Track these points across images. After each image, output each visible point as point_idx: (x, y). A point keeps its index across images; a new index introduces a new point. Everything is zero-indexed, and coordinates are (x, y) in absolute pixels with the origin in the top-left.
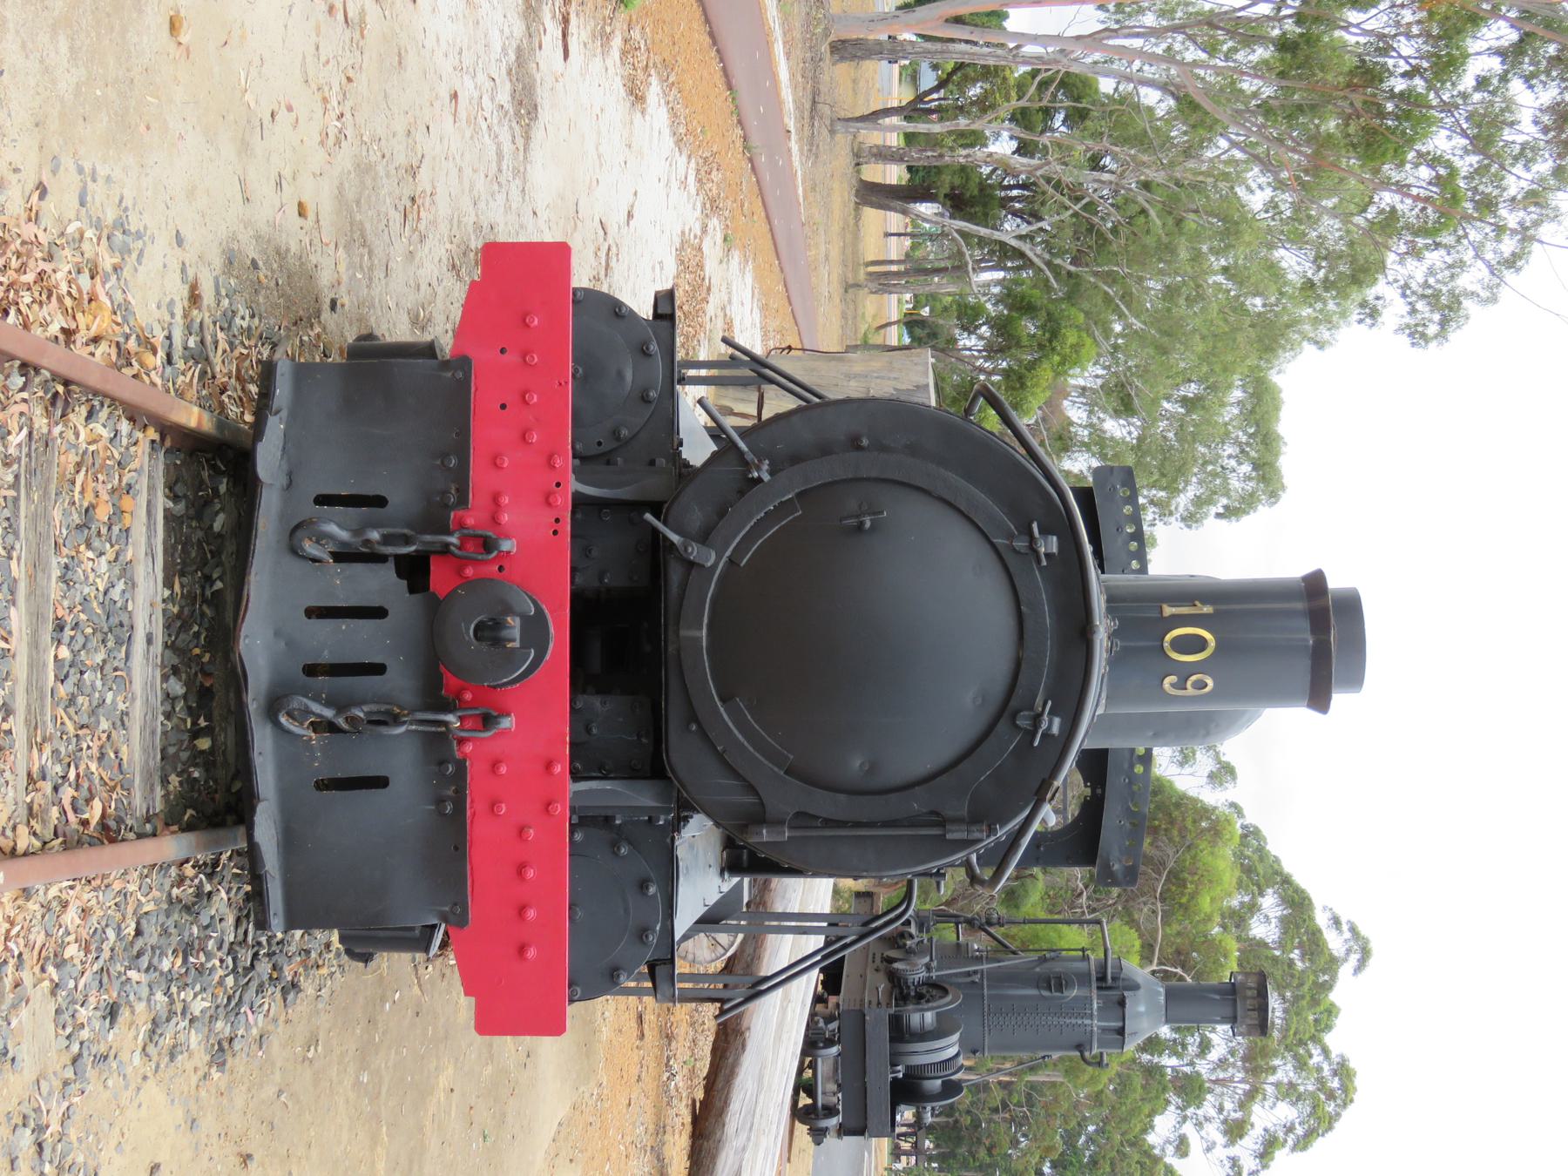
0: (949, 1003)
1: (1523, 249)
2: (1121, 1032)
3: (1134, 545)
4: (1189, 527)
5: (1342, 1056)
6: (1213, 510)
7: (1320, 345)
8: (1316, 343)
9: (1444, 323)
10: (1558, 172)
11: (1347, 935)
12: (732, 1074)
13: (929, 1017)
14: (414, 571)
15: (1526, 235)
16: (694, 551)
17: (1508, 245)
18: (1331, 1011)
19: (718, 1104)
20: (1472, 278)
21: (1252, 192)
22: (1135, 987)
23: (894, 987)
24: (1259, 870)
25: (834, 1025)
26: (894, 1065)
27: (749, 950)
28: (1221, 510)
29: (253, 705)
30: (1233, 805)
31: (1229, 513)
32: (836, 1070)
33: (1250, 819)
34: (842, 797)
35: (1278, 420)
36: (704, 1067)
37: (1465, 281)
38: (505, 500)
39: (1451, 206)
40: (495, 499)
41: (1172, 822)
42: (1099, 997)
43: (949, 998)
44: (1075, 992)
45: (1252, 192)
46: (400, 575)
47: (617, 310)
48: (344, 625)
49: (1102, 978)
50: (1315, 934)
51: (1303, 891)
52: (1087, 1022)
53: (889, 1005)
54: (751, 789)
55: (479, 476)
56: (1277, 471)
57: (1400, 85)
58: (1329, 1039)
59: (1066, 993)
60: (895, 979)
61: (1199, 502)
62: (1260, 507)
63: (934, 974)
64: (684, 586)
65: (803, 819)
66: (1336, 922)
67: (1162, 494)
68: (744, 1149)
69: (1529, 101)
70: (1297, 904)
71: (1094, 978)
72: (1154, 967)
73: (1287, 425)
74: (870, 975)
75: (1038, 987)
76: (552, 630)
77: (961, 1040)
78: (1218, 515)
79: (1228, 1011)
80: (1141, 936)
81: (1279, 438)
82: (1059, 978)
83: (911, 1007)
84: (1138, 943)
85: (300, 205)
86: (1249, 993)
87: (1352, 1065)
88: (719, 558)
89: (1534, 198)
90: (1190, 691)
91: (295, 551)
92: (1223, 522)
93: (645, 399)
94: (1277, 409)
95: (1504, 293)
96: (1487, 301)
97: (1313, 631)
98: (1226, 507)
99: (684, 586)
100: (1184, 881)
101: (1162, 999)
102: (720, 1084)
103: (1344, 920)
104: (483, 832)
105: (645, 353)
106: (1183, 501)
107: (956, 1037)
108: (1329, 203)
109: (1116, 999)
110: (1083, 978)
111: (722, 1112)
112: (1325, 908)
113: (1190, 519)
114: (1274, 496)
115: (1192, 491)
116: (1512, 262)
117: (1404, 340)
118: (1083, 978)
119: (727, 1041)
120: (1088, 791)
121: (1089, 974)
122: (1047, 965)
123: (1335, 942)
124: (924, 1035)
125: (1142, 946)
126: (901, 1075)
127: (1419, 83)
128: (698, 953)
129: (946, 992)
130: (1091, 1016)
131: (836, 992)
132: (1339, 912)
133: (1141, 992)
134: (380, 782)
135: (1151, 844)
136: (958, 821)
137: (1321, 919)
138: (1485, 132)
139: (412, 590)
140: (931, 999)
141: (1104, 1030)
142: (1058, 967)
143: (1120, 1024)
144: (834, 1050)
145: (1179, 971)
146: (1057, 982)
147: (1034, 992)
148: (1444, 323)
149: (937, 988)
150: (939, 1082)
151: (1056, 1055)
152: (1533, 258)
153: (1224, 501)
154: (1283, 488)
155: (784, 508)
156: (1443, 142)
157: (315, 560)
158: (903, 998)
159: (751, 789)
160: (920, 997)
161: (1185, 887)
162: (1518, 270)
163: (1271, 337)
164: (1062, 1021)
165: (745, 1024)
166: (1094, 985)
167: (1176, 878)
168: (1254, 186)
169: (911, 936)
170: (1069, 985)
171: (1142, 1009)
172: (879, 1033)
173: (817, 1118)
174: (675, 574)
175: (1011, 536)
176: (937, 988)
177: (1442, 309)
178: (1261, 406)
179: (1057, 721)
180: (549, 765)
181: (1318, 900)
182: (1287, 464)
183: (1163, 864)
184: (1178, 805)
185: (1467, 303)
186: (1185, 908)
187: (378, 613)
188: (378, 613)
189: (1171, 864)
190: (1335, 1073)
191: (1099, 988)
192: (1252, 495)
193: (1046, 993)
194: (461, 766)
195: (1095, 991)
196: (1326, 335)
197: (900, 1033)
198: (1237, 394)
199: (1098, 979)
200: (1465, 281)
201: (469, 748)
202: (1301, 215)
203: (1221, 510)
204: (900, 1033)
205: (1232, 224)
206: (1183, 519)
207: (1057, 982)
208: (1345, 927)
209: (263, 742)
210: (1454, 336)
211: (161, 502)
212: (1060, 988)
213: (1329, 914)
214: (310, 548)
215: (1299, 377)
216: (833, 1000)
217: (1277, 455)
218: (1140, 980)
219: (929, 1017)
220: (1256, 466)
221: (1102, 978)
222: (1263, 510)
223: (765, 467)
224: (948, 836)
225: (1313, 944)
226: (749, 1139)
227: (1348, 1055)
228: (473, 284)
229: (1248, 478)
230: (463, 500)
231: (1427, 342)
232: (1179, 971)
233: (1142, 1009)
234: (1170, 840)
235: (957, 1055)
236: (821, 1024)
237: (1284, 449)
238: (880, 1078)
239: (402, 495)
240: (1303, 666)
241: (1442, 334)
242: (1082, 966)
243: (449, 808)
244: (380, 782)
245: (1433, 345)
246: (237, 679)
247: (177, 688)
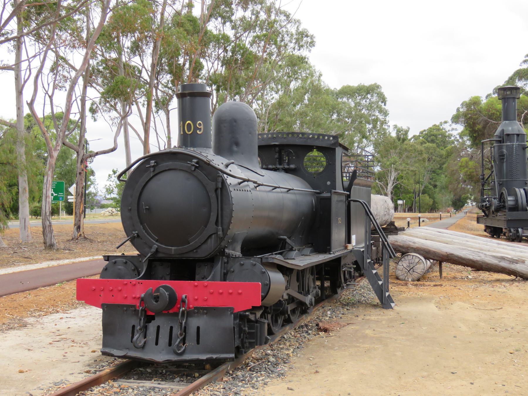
0: (505, 191)
1: (283, 13)
2: (518, 135)
3: (290, 136)
4: (388, 114)
6: (383, 106)
7: (321, 75)
8: (319, 77)
9: (307, 36)
10: (261, 3)
12: (461, 258)
14: (149, 319)
15: (279, 12)
16: (153, 250)
17: (283, 18)
19: (471, 262)
20: (292, 29)
21: (273, 98)
23: (500, 210)
25: (512, 230)
27: (422, 252)
28: (383, 104)
29: (174, 358)
30: (487, 97)
31: (384, 101)
33: (491, 92)
34: (212, 214)
35: (353, 86)
36: (460, 267)
37: (293, 30)
38: (134, 296)
39: (271, 35)
40: (135, 298)
43: (504, 192)
44: (505, 150)
45: (273, 98)
46: (150, 322)
47: (105, 269)
48: (160, 336)
49: (500, 142)
51: (515, 73)
52: (515, 146)
53: (505, 212)
54: (210, 236)
55: (129, 302)
56: (370, 86)
57: (230, 54)
59: (505, 153)
61: (381, 111)
62: (382, 91)
63: (497, 197)
64: (164, 253)
65: (217, 223)
67: (378, 123)
68: (485, 254)
69: (239, 13)
73: (354, 83)
74: (498, 218)
75: (503, 162)
76: (170, 286)
77: (519, 188)
78: (385, 105)
79: (511, 100)
81: (359, 86)
82: (500, 156)
83: (506, 205)
85: (92, 352)
86: (505, 93)
88: (155, 244)
89: (269, 11)
90: (202, 127)
91: (143, 347)
92: (387, 103)
93: (126, 263)
94: (349, 87)
95: (296, 17)
96: (300, 23)
97: (186, 97)
98: (382, 102)
99: (164, 253)
100: (491, 114)
101: (507, 122)
102: (465, 262)
103: (525, 59)
104: (212, 303)
105: (115, 262)
106: (381, 117)
107: (517, 190)
108: (275, 74)
110: (500, 148)
111: (473, 261)
112: (520, 65)
113: (386, 114)
114: (378, 87)
115: (377, 113)
116: (287, 16)
117: (313, 49)
118: (500, 148)
119: (451, 259)
120: (315, 150)
124: (516, 200)
127: (229, 48)
128: (422, 268)
129: (502, 193)
133: (505, 129)
134: (198, 328)
136: (216, 185)
138: (248, 26)
139: (154, 319)
141: (517, 141)
142: (497, 156)
144: (520, 230)
145: (523, 115)
147: (505, 164)
148: (307, 36)
152: (286, 10)
153: (380, 103)
154: (375, 84)
155: (144, 228)
156: (247, 39)
157: (145, 343)
158: (504, 207)
159: (210, 236)
160: (504, 202)
161: (494, 113)
162: (290, 14)
163: (317, 90)
165: (445, 254)
167: (491, 116)
168: (272, 97)
169: (486, 205)
170: (502, 152)
171: (510, 128)
172: (516, 215)
174: (160, 255)
175: (150, 172)
177: (303, 38)
178: (348, 92)
179: (193, 160)
180: (196, 286)
181: (518, 68)
182: (367, 82)
183: (486, 120)
185: (301, 29)
187: (158, 327)
188: (158, 327)
189: (486, 118)
191: (503, 142)
192: (378, 94)
193: (505, 160)
194: (195, 308)
195: (504, 144)
196: (318, 74)
198: (345, 99)
200: (293, 30)
201: (191, 306)
202: (278, 81)
203: (383, 104)
204: (515, 208)
205: (280, 105)
206: (386, 116)
207: (502, 156)
209: (187, 357)
210: (310, 33)
211: (132, 380)
213: (523, 64)
214: (141, 344)
215: (332, 80)
216: (504, 230)
217: (364, 86)
219: (509, 198)
220: (368, 93)
221: (500, 142)
222: (383, 90)
223: (134, 232)
224: (220, 187)
226: (482, 253)
228: (86, 303)
229: (372, 96)
230: (134, 306)
231: (313, 42)
232: (523, 115)
233: (510, 128)
235: (524, 189)
236: (511, 234)
237: (362, 84)
239: (133, 321)
240: (199, 100)
241: (312, 37)
242: (496, 148)
243: (205, 311)
244: (198, 328)
245: (315, 40)
246: (169, 362)
247: (178, 379)
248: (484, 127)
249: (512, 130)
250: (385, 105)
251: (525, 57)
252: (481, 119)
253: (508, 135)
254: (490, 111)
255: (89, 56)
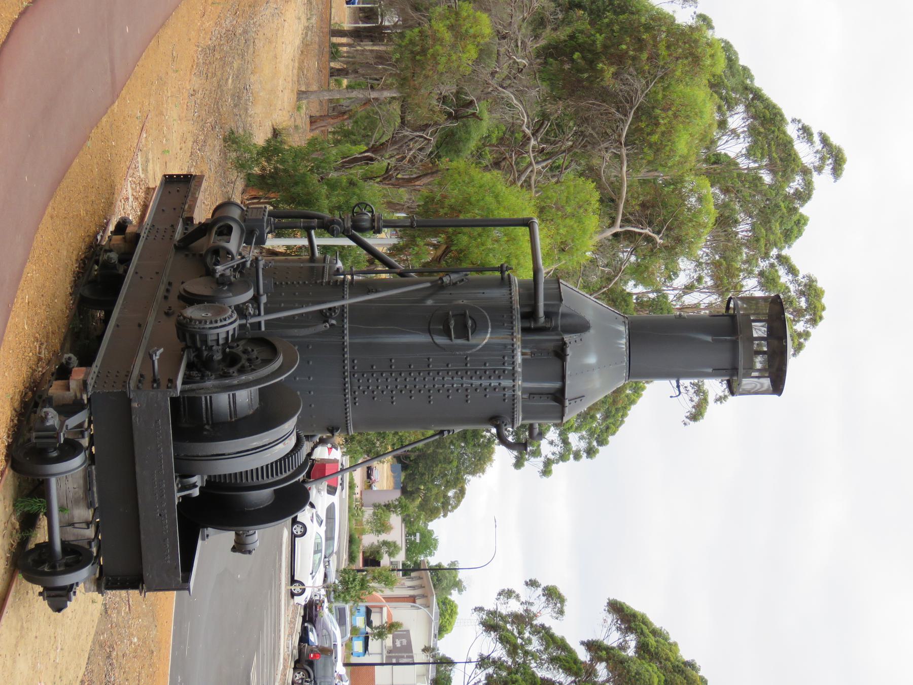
2: (559, 396)
5: (809, 277)
11: (818, 145)
13: (245, 398)
18: (801, 222)
22: (581, 327)
24: (732, 83)
26: (184, 475)
32: (88, 489)
41: (640, 45)
42: (525, 344)
44: (487, 338)
49: (530, 315)
50: (786, 145)
51: (774, 107)
58: (796, 252)
59: (473, 340)
60: (187, 334)
66: (806, 131)
70: (766, 120)
71: (517, 315)
72: (617, 229)
75: (430, 332)
79: (724, 358)
80: (599, 187)
82: (462, 317)
84: (597, 195)
87: (820, 284)
100: (656, 118)
101: (623, 342)
103: (815, 131)
109: (550, 346)
118: (500, 316)
121: (511, 309)
122: (444, 295)
123: (806, 153)
125: (601, 201)
126: (196, 492)
130: (513, 375)
131: (86, 360)
132: (806, 122)
135: (616, 75)
137: (791, 130)
140: (252, 366)
141: (532, 394)
143: (558, 385)
146: (462, 323)
147: (422, 338)
149: (258, 345)
150: (268, 492)
151: (458, 429)
158: (200, 366)
160: (231, 360)
161: (657, 124)
164: (466, 382)
166: (518, 325)
167: (646, 113)
171: (592, 360)
173: (55, 573)
176: (258, 345)
181: (788, 115)
183: (630, 101)
184: (648, 28)
186: (657, 149)
190: (802, 293)
191: (525, 330)
193: (441, 340)
197: (194, 424)
199: (525, 316)
206: (580, 451)
208: (816, 138)
212: (463, 333)
218: (589, 315)
225: (783, 160)
227: (815, 275)
232: (647, 231)
234: (640, 71)
238: (164, 493)
242: (497, 294)
248: (605, 95)
249: (587, 370)
250: (794, 355)
251: (821, 134)
252: (638, 84)
253: (560, 353)
254: (665, 110)
255: (504, 633)
